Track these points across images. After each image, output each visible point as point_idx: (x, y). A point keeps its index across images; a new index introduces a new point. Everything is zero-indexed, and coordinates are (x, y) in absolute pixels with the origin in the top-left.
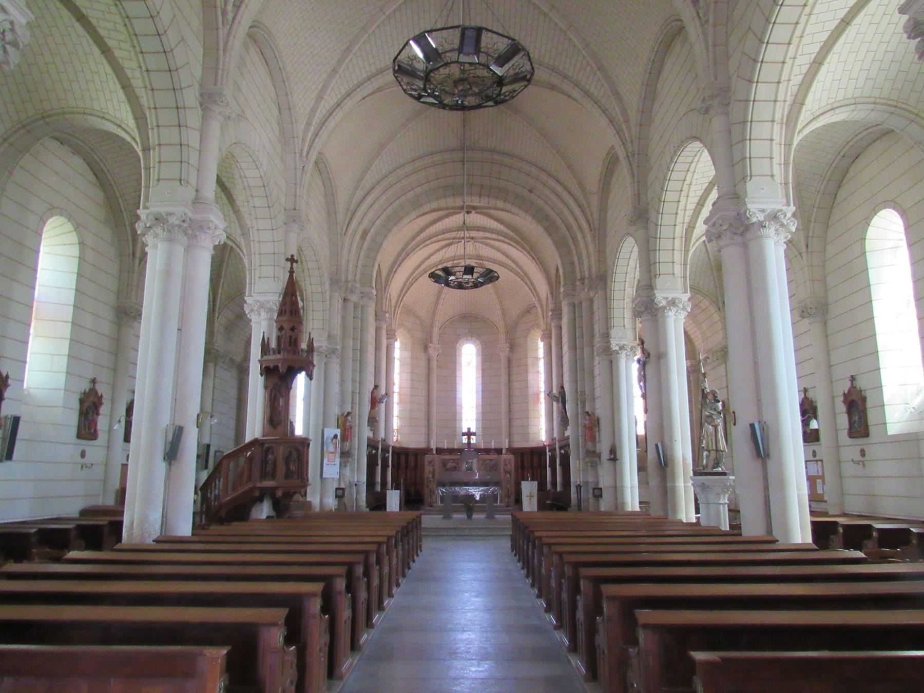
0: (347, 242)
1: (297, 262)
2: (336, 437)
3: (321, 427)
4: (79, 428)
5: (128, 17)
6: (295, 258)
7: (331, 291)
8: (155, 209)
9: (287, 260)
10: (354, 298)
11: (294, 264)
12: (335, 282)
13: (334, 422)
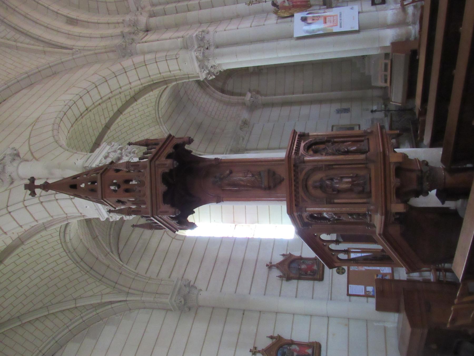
0: (81, 43)
1: (32, 180)
2: (304, 19)
3: (294, 42)
4: (314, 279)
5: (81, 115)
6: (28, 182)
7: (132, 54)
8: (198, 70)
9: (33, 194)
10: (143, 19)
11: (37, 183)
12: (125, 51)
13: (283, 26)
